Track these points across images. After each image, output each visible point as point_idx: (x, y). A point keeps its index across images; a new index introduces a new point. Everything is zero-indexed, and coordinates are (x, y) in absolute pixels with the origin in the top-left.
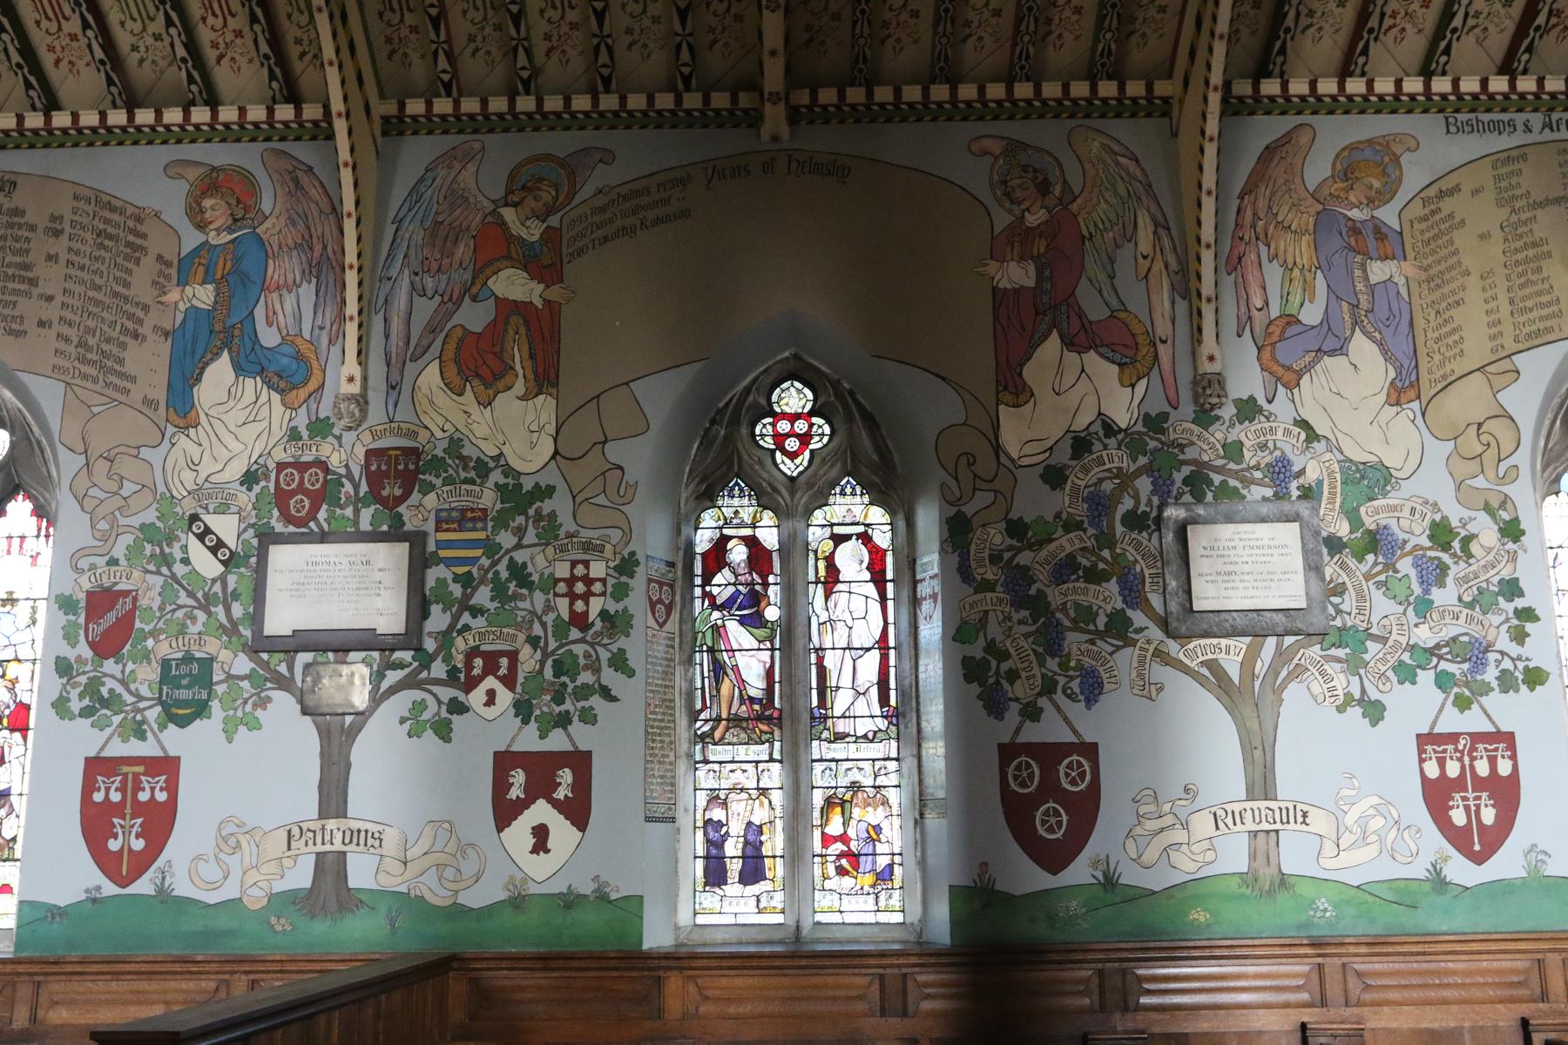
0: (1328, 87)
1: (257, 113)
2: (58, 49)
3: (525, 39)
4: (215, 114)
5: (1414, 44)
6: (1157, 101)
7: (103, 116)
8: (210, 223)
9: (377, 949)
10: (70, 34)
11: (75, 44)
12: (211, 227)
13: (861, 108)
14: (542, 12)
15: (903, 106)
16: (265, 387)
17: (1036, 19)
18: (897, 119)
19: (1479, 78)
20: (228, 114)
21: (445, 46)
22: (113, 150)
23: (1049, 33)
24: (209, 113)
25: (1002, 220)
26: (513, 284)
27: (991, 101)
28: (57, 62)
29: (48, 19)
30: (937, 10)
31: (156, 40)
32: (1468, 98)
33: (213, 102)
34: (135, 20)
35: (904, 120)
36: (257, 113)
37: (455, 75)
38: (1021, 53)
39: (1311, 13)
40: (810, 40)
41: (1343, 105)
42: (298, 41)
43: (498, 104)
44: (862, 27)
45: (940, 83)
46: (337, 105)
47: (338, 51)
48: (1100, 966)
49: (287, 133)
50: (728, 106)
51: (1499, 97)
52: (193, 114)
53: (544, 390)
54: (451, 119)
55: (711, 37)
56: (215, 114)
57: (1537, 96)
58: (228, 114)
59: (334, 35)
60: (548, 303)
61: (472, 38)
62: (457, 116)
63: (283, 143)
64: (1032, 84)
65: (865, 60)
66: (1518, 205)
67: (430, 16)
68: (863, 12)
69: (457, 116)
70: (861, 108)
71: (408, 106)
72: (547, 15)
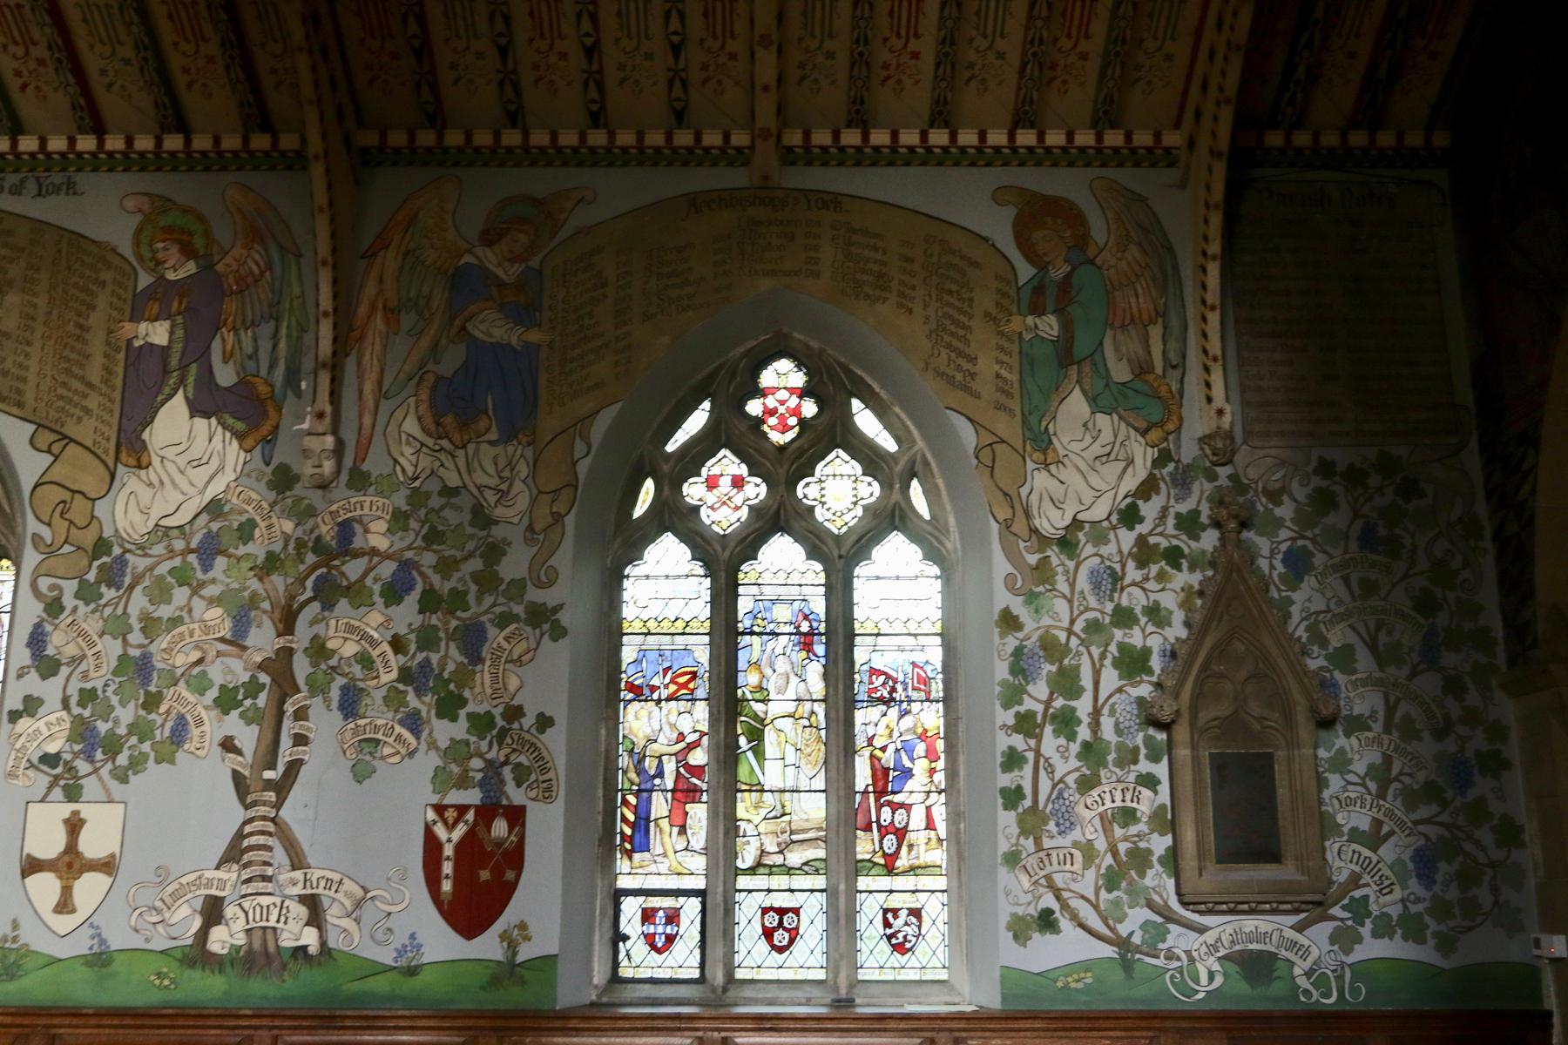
0: (483, 138)
1: (144, 143)
2: (25, 73)
3: (683, 70)
4: (101, 143)
5: (920, 98)
6: (196, 155)
7: (72, 141)
8: (164, 262)
9: (220, 1005)
10: (37, 59)
11: (42, 70)
12: (166, 266)
13: (601, 151)
14: (617, 41)
15: (901, 150)
16: (220, 428)
17: (1041, 65)
18: (526, 163)
19: (976, 131)
20: (115, 143)
21: (597, 76)
22: (963, 171)
23: (1053, 79)
24: (95, 142)
25: (145, 280)
26: (492, 328)
27: (567, 147)
28: (24, 87)
29: (101, 41)
30: (1024, 54)
31: (39, 65)
32: (26, 157)
33: (100, 131)
34: (104, 44)
35: (533, 164)
36: (231, 143)
37: (603, 108)
38: (1025, 97)
39: (1054, 66)
40: (624, 80)
41: (497, 156)
42: (274, 71)
43: (1085, 138)
44: (1032, 70)
45: (939, 128)
46: (314, 137)
47: (317, 85)
48: (700, 1034)
49: (1116, 158)
50: (800, 143)
51: (851, 151)
52: (21, 143)
53: (250, 441)
54: (212, 155)
55: (885, 73)
56: (101, 143)
57: (979, 149)
58: (115, 143)
59: (314, 68)
60: (527, 344)
61: (18, 73)
62: (1099, 150)
63: (1104, 169)
64: (1034, 131)
65: (1032, 102)
66: (876, 268)
67: (583, 45)
68: (1117, 54)
69: (1099, 150)
70: (118, 156)
71: (618, 137)
72: (889, 44)
